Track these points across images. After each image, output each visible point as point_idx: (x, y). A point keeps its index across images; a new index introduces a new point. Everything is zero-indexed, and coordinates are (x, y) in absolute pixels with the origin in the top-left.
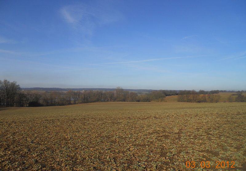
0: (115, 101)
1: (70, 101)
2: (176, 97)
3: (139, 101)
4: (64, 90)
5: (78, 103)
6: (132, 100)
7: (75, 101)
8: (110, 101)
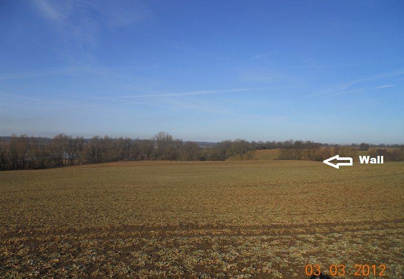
0: (156, 160)
1: (60, 158)
2: (277, 151)
3: (203, 159)
4: (388, 146)
5: (78, 164)
6: (191, 158)
7: (71, 159)
8: (147, 160)
